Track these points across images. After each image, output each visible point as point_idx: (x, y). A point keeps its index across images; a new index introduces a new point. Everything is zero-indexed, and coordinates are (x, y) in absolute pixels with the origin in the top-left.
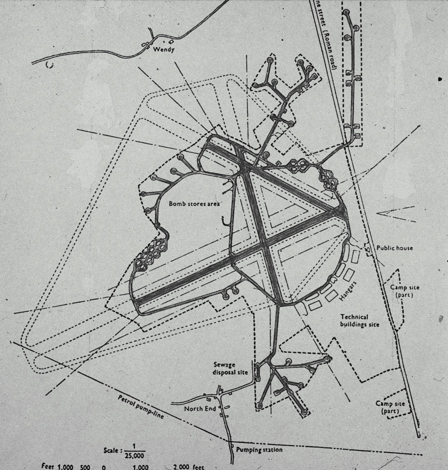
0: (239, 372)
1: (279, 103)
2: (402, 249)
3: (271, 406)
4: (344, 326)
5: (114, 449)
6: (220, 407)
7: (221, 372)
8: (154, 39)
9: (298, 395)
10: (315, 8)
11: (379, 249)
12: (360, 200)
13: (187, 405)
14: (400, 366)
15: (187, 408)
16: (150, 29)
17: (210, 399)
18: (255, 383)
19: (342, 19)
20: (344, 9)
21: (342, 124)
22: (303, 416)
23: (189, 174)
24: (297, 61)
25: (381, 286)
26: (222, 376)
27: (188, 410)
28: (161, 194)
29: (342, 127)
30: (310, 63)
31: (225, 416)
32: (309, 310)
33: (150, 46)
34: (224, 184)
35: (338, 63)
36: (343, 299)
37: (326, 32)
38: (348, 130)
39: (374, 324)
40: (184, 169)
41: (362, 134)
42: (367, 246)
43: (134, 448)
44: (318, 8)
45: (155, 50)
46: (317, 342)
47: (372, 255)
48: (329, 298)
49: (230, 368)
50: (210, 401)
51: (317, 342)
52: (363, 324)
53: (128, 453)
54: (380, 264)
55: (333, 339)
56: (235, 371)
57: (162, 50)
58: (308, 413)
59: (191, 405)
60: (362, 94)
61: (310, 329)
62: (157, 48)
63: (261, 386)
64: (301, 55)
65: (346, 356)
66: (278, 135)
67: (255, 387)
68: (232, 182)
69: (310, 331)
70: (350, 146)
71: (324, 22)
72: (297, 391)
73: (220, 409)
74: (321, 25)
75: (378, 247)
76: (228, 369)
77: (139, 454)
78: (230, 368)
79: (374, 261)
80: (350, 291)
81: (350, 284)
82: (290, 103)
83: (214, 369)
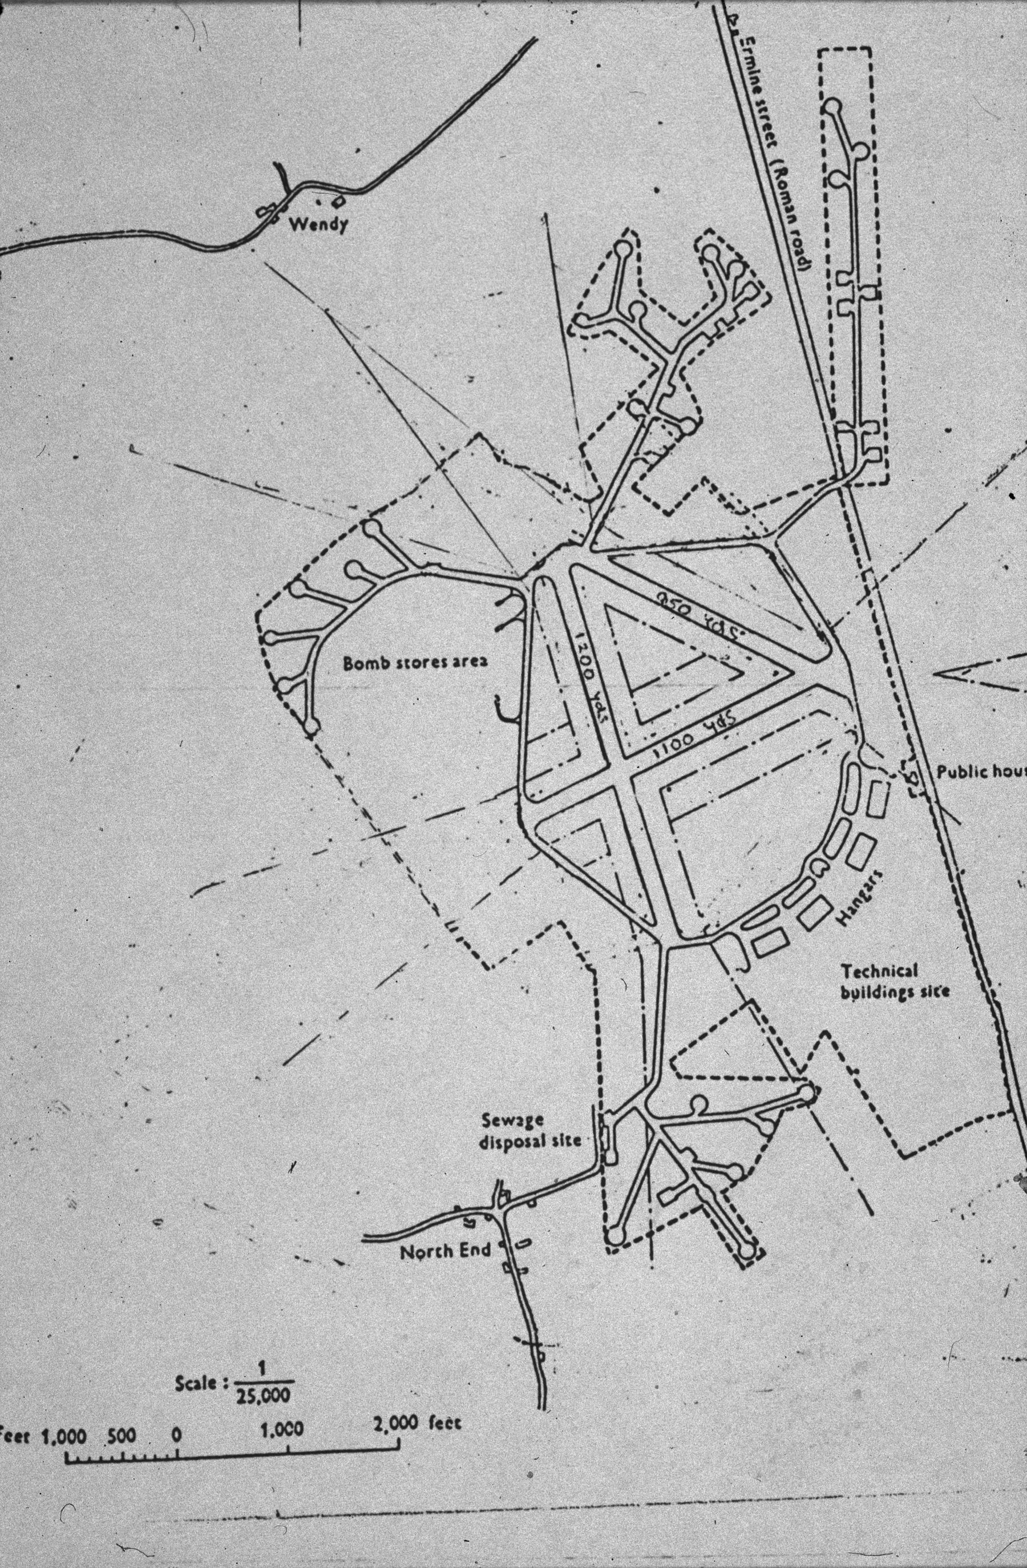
0: (555, 1139)
1: (653, 368)
2: (1008, 773)
3: (650, 1235)
4: (851, 998)
5: (204, 1377)
6: (502, 1244)
7: (502, 1143)
8: (291, 193)
9: (727, 1200)
10: (747, 95)
11: (943, 775)
12: (885, 636)
13: (407, 1243)
14: (1011, 1105)
15: (408, 1249)
16: (279, 167)
17: (474, 1221)
18: (602, 1170)
19: (823, 125)
20: (825, 98)
21: (830, 424)
22: (745, 1263)
23: (396, 578)
24: (700, 248)
25: (951, 880)
26: (506, 1152)
27: (411, 1256)
28: (316, 639)
29: (831, 433)
30: (737, 254)
31: (518, 1270)
32: (754, 954)
33: (280, 215)
34: (499, 603)
35: (814, 251)
36: (846, 920)
37: (778, 166)
38: (846, 441)
39: (936, 989)
40: (383, 563)
41: (886, 448)
42: (911, 767)
43: (263, 1373)
44: (755, 98)
45: (294, 228)
46: (777, 1044)
47: (924, 793)
48: (809, 919)
49: (529, 1128)
50: (473, 1227)
51: (777, 1044)
52: (902, 991)
53: (246, 1388)
54: (946, 817)
55: (821, 1036)
56: (543, 1136)
57: (313, 226)
58: (758, 1253)
59: (419, 1241)
60: (882, 336)
61: (759, 1010)
62: (299, 220)
63: (621, 1177)
64: (710, 231)
65: (858, 1084)
66: (652, 459)
67: (603, 1182)
68: (523, 597)
69: (759, 1016)
70: (853, 483)
71: (772, 136)
72: (726, 1190)
73: (503, 1250)
74: (765, 146)
75: (941, 769)
76: (523, 1133)
77: (276, 1389)
78: (529, 1128)
79: (931, 809)
80: (864, 897)
81: (864, 877)
82: (684, 368)
83: (482, 1133)
